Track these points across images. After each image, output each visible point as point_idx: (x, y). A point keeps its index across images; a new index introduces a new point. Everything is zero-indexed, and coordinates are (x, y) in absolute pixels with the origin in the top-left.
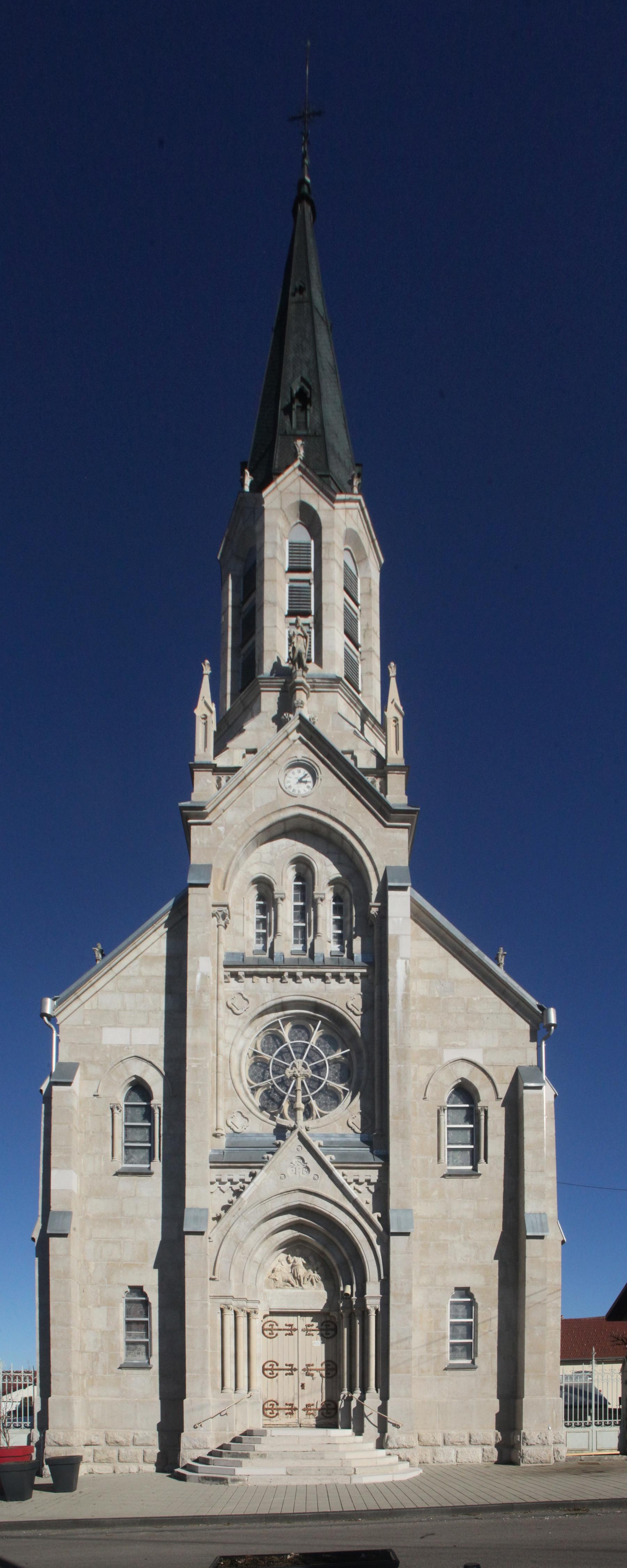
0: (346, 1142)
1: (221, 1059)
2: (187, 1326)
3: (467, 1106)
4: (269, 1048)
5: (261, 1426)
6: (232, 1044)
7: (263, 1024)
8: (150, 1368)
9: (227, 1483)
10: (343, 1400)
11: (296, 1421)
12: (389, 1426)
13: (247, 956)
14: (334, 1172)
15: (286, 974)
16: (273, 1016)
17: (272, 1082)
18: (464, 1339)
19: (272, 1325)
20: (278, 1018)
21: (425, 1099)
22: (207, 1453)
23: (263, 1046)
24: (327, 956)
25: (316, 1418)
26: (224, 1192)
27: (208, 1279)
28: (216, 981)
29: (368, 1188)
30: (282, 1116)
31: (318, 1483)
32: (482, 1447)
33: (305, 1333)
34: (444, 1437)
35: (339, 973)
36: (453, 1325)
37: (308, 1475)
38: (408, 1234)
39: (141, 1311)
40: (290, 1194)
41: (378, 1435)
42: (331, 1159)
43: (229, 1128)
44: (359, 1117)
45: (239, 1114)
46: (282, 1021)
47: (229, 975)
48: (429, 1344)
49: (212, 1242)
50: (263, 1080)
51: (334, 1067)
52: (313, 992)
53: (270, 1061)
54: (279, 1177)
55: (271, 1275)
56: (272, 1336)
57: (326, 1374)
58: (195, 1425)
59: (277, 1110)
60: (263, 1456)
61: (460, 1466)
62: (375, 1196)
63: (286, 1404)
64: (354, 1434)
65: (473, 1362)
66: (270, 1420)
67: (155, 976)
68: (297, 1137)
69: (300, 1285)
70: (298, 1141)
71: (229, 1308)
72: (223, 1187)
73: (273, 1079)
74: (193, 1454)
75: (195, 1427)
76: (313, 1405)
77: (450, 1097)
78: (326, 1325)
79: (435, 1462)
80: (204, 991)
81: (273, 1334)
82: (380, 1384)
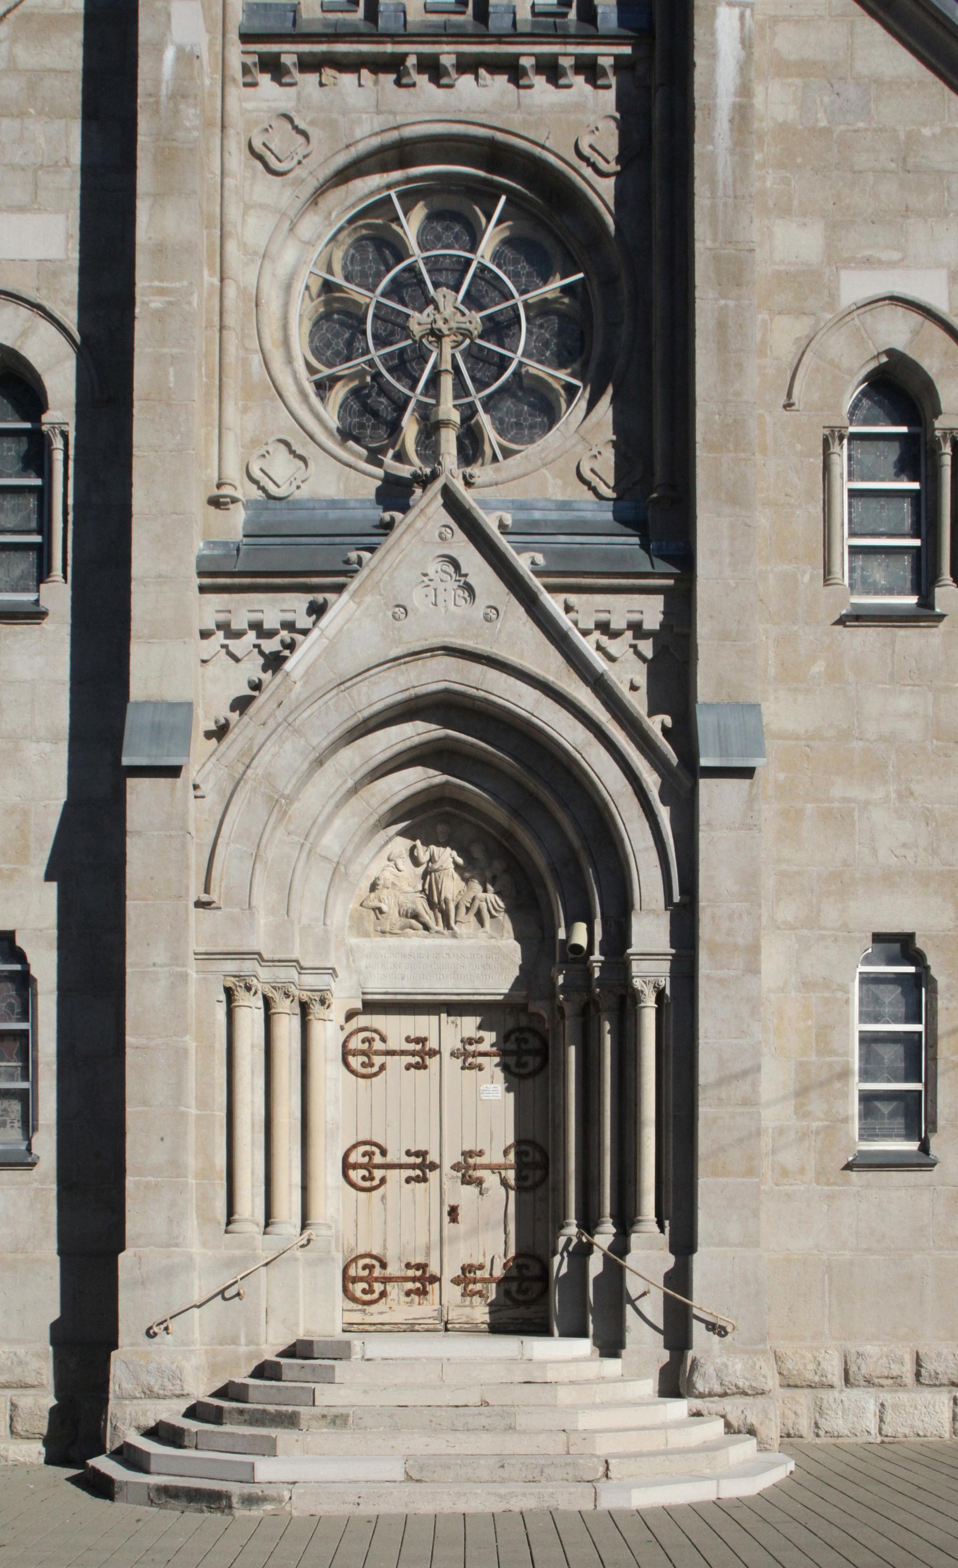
0: (572, 523)
1: (231, 291)
2: (129, 1039)
3: (904, 429)
4: (364, 275)
5: (339, 1327)
6: (264, 257)
7: (348, 203)
8: (33, 1164)
9: (230, 1507)
10: (565, 1254)
11: (435, 1314)
12: (698, 1331)
13: (305, 15)
14: (541, 598)
15: (411, 61)
16: (376, 180)
17: (371, 363)
18: (897, 1080)
19: (369, 1041)
20: (389, 187)
21: (788, 406)
22: (183, 1410)
23: (350, 268)
24: (524, 14)
25: (490, 1305)
26: (237, 660)
27: (192, 905)
28: (218, 77)
29: (634, 647)
30: (400, 457)
31: (498, 1507)
32: (950, 1392)
33: (459, 1062)
34: (846, 1362)
35: (555, 56)
36: (867, 1040)
37: (469, 1480)
38: (747, 773)
39: (10, 1003)
40: (420, 662)
41: (665, 1356)
42: (533, 563)
43: (255, 487)
44: (609, 455)
45: (282, 447)
46: (401, 196)
47: (255, 64)
48: (802, 1092)
49: (203, 797)
50: (348, 359)
51: (541, 326)
52: (485, 112)
53: (368, 306)
54: (390, 614)
55: (368, 897)
56: (369, 1071)
57: (518, 1178)
58: (151, 1328)
59: (386, 442)
60: (338, 1420)
61: (888, 1446)
62: (655, 668)
63: (408, 1266)
64: (598, 1352)
65: (925, 1148)
66: (364, 1311)
67: (54, 70)
68: (440, 500)
69: (447, 925)
70: (443, 511)
71: (248, 989)
72: (236, 646)
73: (375, 354)
74: (144, 1413)
75: (150, 1334)
76: (481, 1267)
77: (855, 406)
78: (518, 1040)
79: (822, 1433)
80: (184, 97)
81: (372, 1065)
82: (669, 1207)
